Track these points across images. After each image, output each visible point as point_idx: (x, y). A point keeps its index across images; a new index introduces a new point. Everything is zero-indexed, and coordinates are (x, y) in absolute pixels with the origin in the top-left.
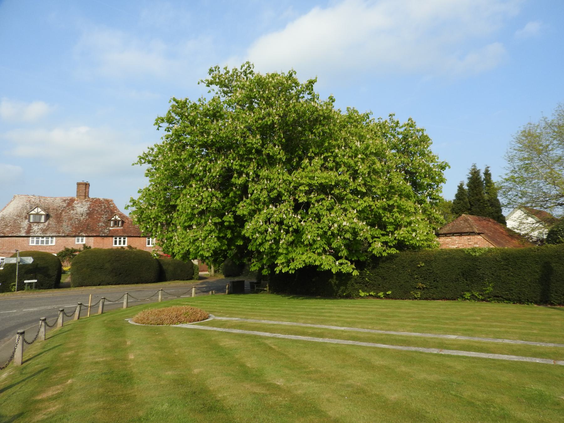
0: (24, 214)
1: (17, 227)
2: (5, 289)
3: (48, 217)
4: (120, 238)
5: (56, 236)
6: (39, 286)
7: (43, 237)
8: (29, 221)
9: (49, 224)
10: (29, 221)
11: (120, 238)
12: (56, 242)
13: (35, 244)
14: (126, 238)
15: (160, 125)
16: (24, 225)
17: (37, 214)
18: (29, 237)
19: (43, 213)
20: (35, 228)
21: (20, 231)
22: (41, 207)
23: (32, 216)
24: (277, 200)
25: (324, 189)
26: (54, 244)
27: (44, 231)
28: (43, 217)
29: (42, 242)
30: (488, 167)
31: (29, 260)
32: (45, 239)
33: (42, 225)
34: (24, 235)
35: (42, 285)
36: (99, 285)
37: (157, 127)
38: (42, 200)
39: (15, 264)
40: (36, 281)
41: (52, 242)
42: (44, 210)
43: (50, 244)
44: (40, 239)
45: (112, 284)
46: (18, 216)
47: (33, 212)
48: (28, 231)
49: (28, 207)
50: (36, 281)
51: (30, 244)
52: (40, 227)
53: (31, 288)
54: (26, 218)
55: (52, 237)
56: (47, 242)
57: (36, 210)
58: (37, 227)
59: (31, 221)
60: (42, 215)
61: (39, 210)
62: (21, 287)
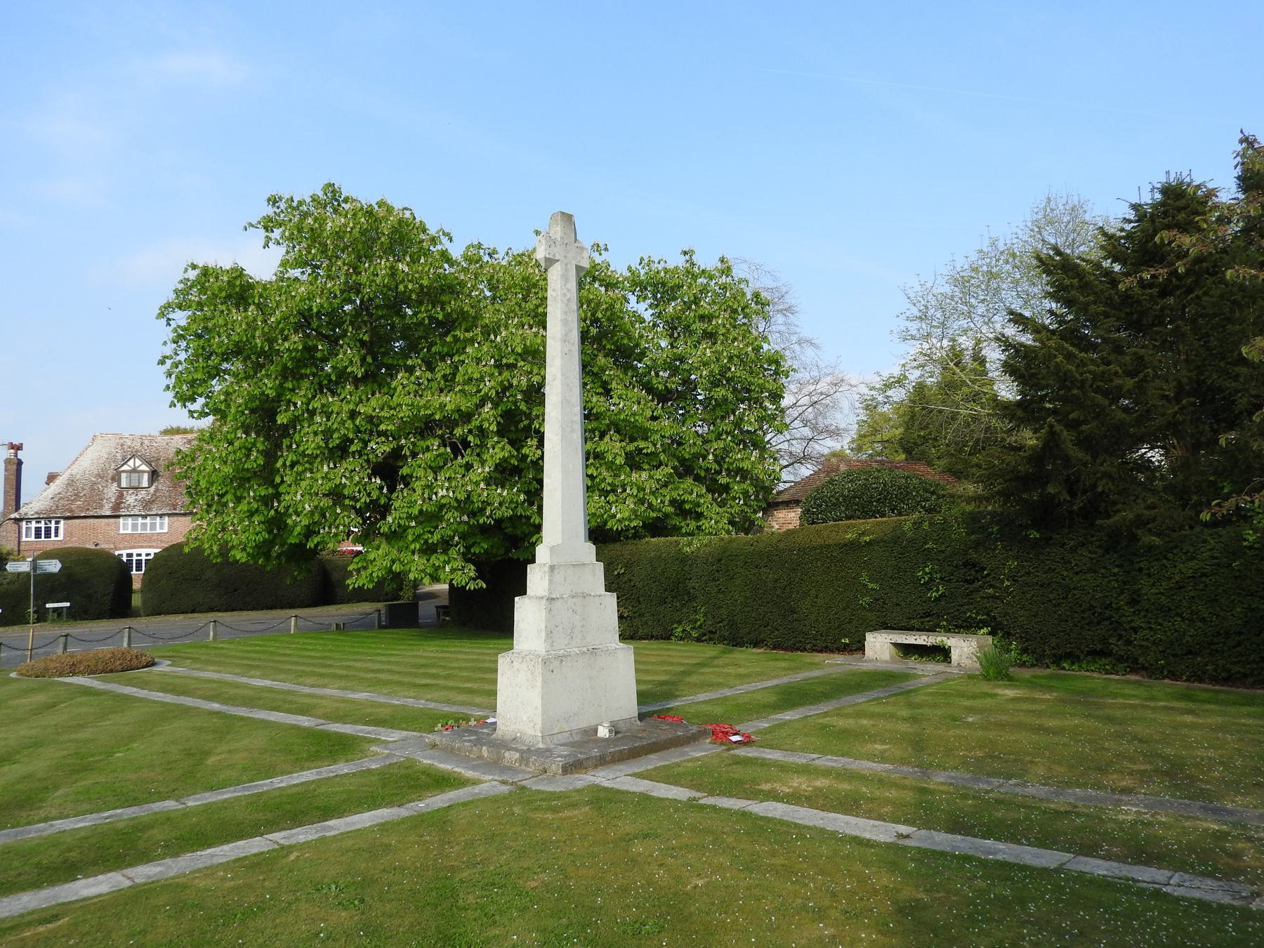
0: (111, 473)
1: (95, 496)
2: (15, 617)
3: (154, 475)
4: (57, 523)
5: (169, 515)
6: (75, 615)
7: (145, 517)
8: (119, 485)
9: (157, 490)
10: (119, 485)
11: (57, 523)
12: (170, 526)
13: (129, 531)
14: (62, 522)
15: (170, 316)
16: (110, 494)
17: (134, 470)
18: (118, 517)
19: (144, 468)
20: (130, 499)
21: (101, 507)
22: (140, 457)
23: (124, 475)
24: (340, 452)
25: (426, 427)
26: (165, 530)
27: (147, 504)
28: (146, 476)
29: (144, 525)
30: (18, 448)
31: (54, 566)
32: (148, 520)
33: (143, 492)
34: (108, 513)
35: (85, 612)
36: (193, 612)
37: (164, 321)
38: (146, 442)
39: (28, 574)
40: (68, 604)
41: (162, 527)
42: (149, 463)
43: (158, 531)
44: (140, 520)
45: (219, 611)
46: (98, 475)
47: (125, 468)
48: (117, 506)
49: (119, 456)
50: (68, 604)
51: (122, 531)
52: (140, 497)
53: (59, 615)
54: (113, 479)
55: (161, 516)
56: (153, 526)
57: (131, 463)
58: (134, 497)
59: (124, 485)
60: (143, 472)
61: (138, 462)
62: (42, 616)
